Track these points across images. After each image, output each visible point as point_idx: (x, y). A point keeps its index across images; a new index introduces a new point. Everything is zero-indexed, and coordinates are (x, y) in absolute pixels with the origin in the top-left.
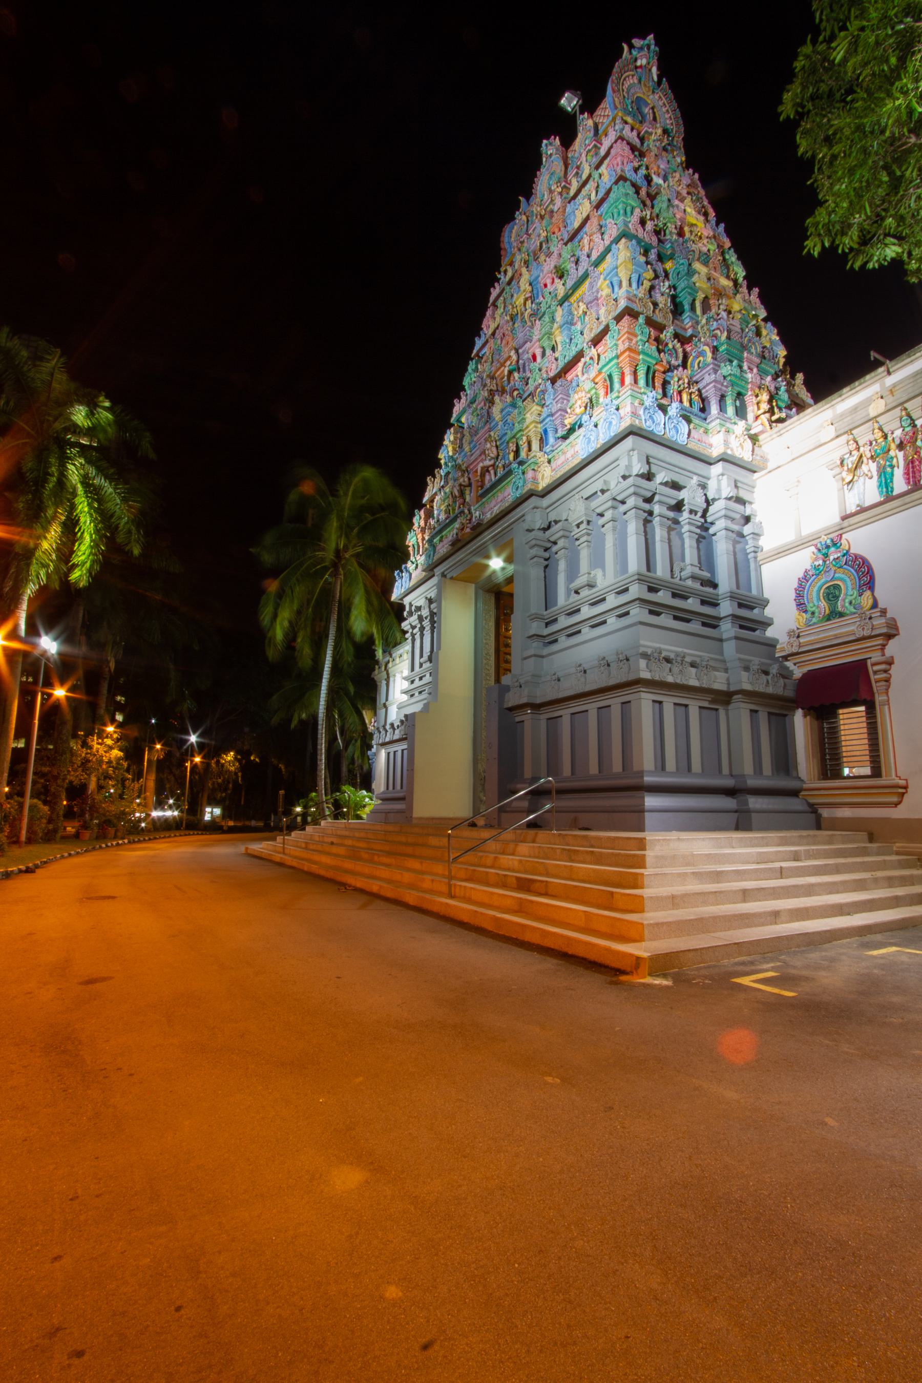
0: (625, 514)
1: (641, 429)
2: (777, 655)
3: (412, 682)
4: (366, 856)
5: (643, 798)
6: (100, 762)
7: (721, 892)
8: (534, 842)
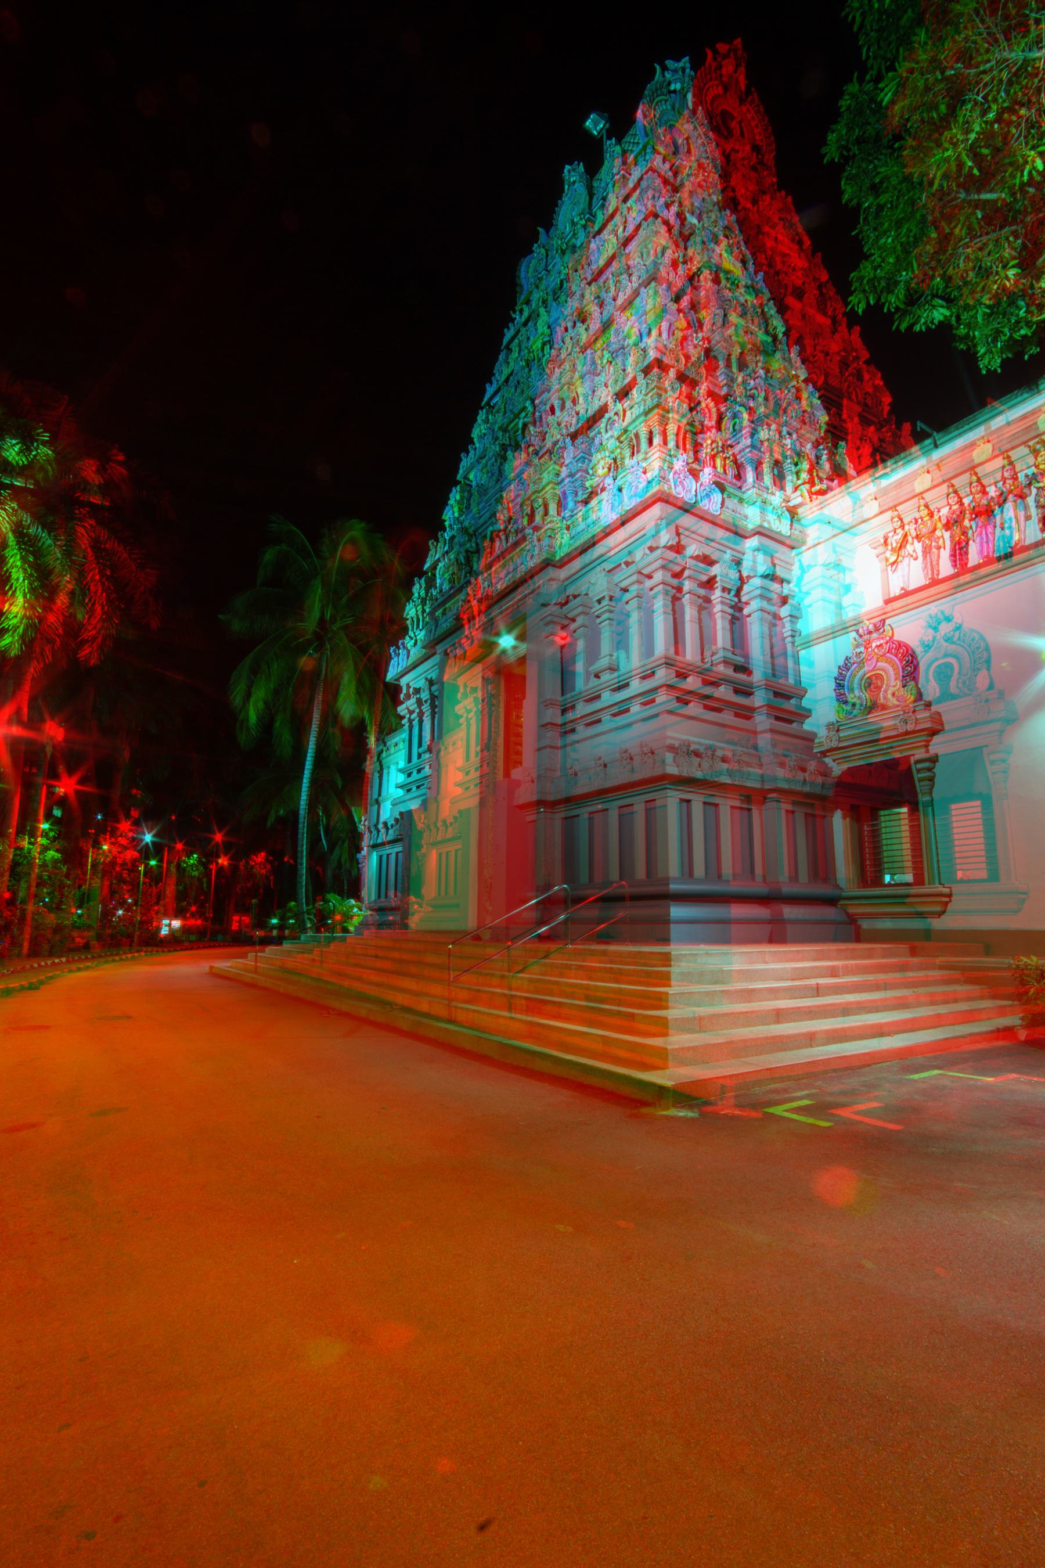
1: (670, 495)
2: (815, 751)
3: (409, 775)
5: (669, 908)
7: (753, 1012)
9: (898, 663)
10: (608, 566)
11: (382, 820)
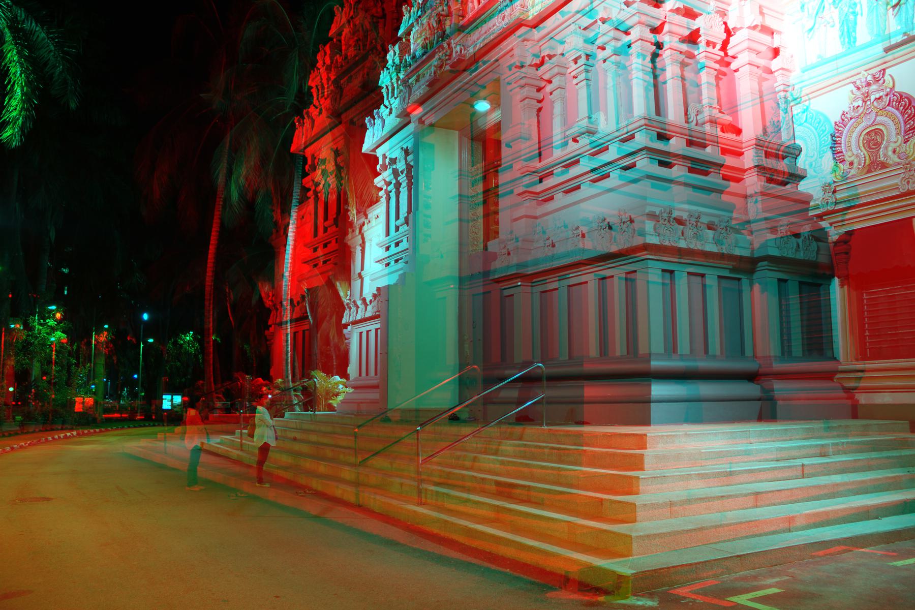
2: (811, 213)
3: (388, 249)
5: (650, 386)
6: (44, 344)
7: (728, 497)
8: (520, 439)
9: (899, 116)
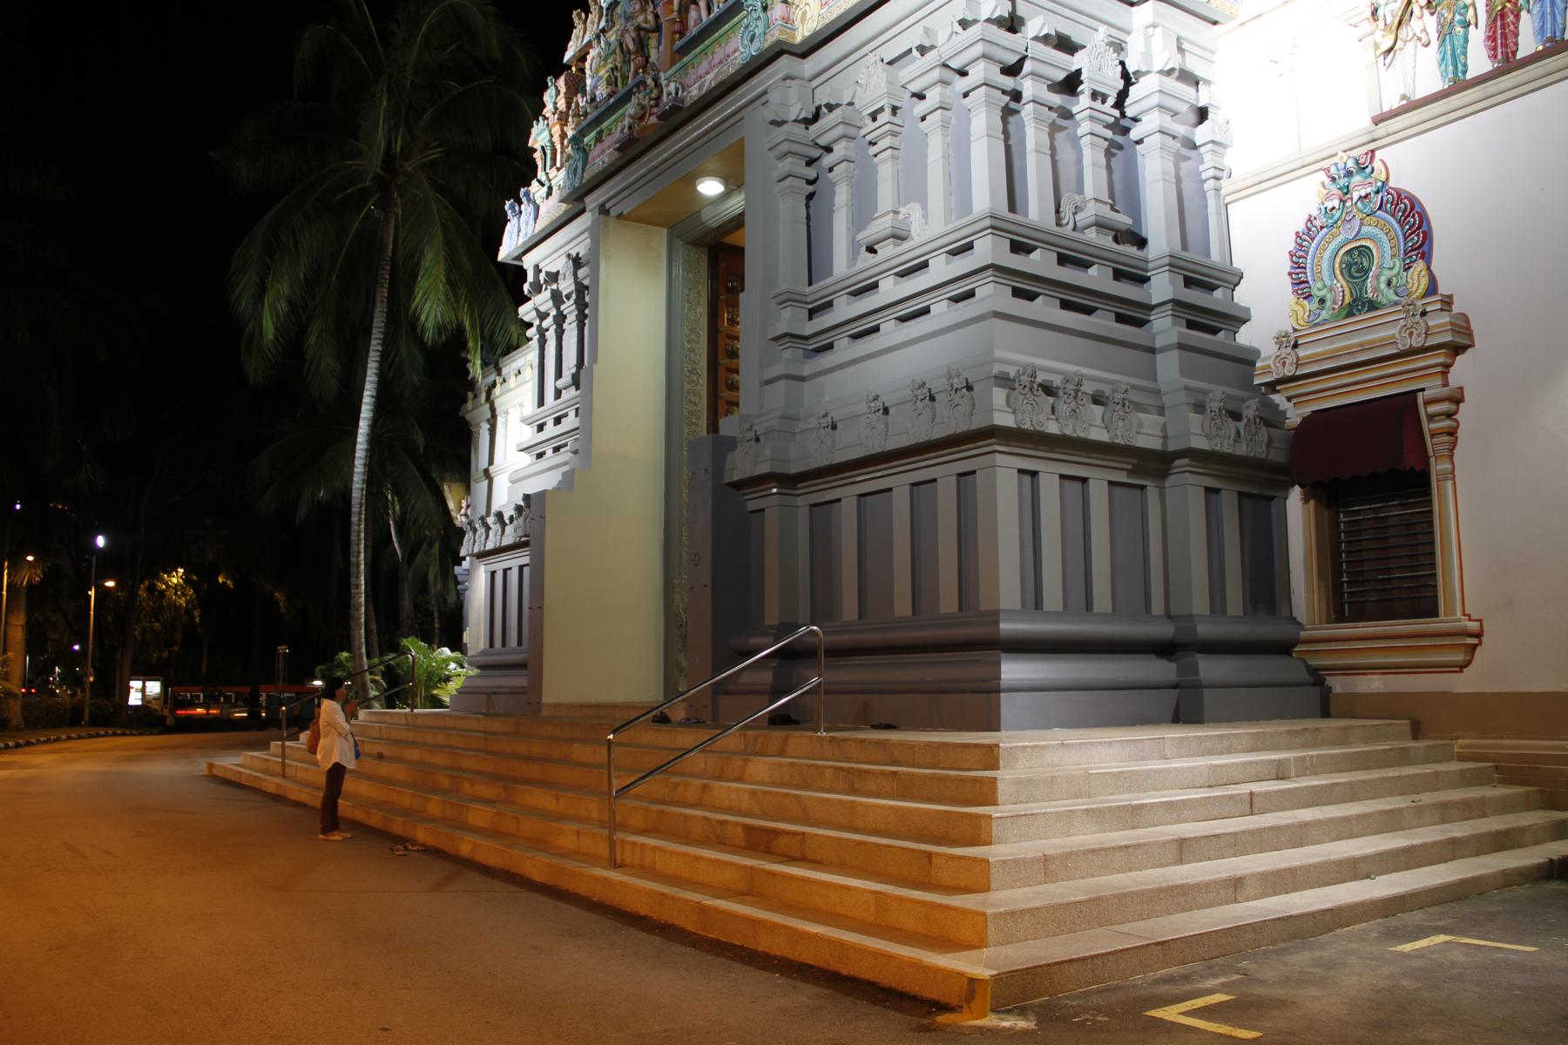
0: (966, 95)
3: (541, 428)
4: (445, 782)
7: (1138, 846)
8: (781, 753)
9: (1397, 226)
10: (891, 52)
11: (495, 508)
